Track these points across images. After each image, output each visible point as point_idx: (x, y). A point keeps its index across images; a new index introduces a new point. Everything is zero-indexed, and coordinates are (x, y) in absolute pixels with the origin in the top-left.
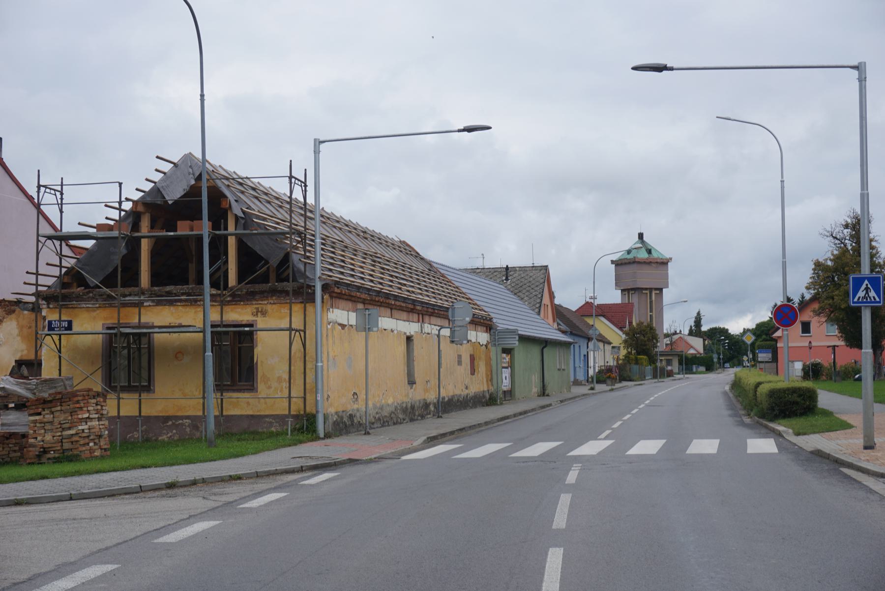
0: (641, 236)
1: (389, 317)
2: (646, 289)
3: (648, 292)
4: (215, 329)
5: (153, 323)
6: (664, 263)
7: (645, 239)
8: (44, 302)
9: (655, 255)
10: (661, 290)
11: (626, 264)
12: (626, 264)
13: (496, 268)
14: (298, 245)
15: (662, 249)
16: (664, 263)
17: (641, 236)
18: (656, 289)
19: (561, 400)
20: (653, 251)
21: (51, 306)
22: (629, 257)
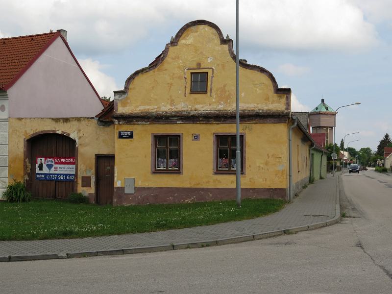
0: (323, 101)
1: (335, 118)
2: (325, 127)
3: (326, 128)
4: (238, 138)
5: (69, 134)
6: (334, 114)
7: (325, 102)
8: (116, 121)
9: (330, 110)
10: (332, 128)
11: (315, 114)
12: (315, 114)
13: (45, 259)
14: (276, 197)
15: (332, 108)
16: (334, 114)
17: (323, 101)
18: (330, 127)
19: (306, 188)
20: (329, 108)
21: (121, 123)
22: (317, 111)
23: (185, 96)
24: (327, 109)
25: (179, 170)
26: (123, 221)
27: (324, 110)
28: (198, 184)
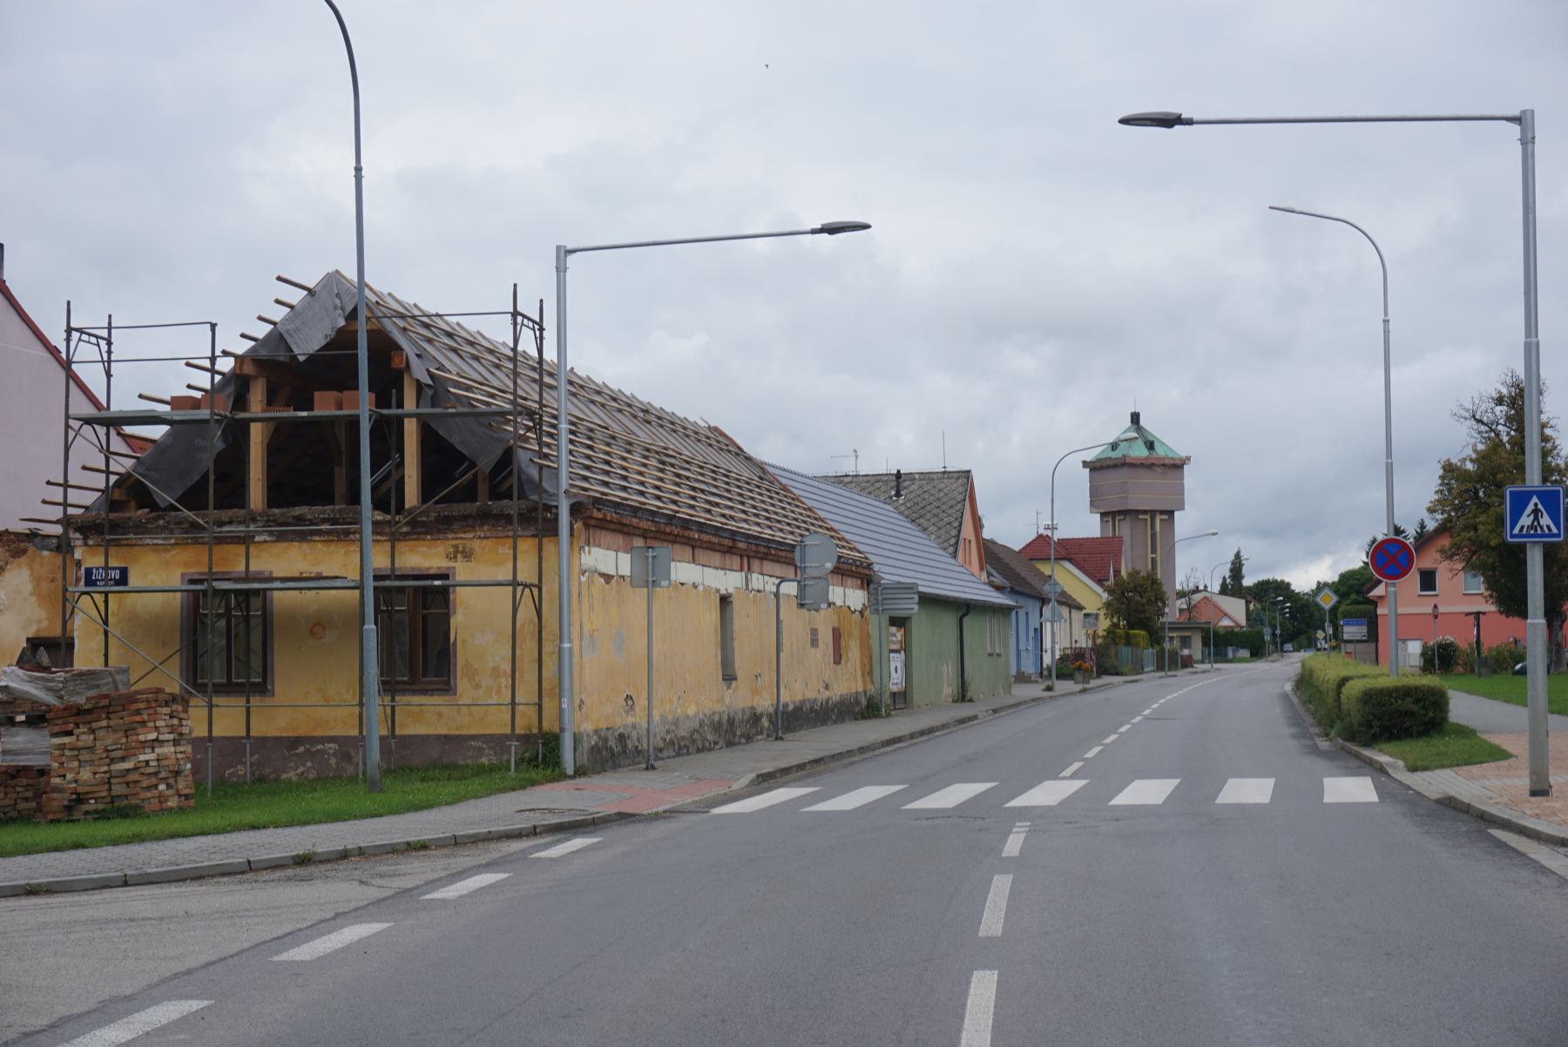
0: (1135, 418)
2: (1145, 512)
3: (1148, 517)
4: (381, 583)
5: (271, 572)
6: (1176, 466)
8: (78, 535)
9: (1160, 451)
10: (1171, 513)
11: (1108, 467)
12: (1108, 467)
15: (1173, 442)
16: (1176, 466)
17: (1135, 418)
18: (1162, 512)
20: (1157, 445)
21: (91, 542)
22: (1114, 455)
23: (855, 451)
24: (1150, 445)
25: (448, 683)
26: (753, 731)
27: (1139, 452)
28: (457, 729)
